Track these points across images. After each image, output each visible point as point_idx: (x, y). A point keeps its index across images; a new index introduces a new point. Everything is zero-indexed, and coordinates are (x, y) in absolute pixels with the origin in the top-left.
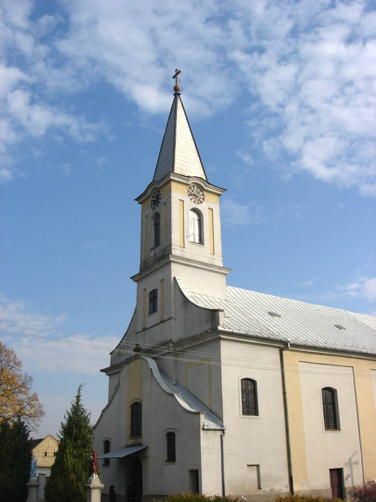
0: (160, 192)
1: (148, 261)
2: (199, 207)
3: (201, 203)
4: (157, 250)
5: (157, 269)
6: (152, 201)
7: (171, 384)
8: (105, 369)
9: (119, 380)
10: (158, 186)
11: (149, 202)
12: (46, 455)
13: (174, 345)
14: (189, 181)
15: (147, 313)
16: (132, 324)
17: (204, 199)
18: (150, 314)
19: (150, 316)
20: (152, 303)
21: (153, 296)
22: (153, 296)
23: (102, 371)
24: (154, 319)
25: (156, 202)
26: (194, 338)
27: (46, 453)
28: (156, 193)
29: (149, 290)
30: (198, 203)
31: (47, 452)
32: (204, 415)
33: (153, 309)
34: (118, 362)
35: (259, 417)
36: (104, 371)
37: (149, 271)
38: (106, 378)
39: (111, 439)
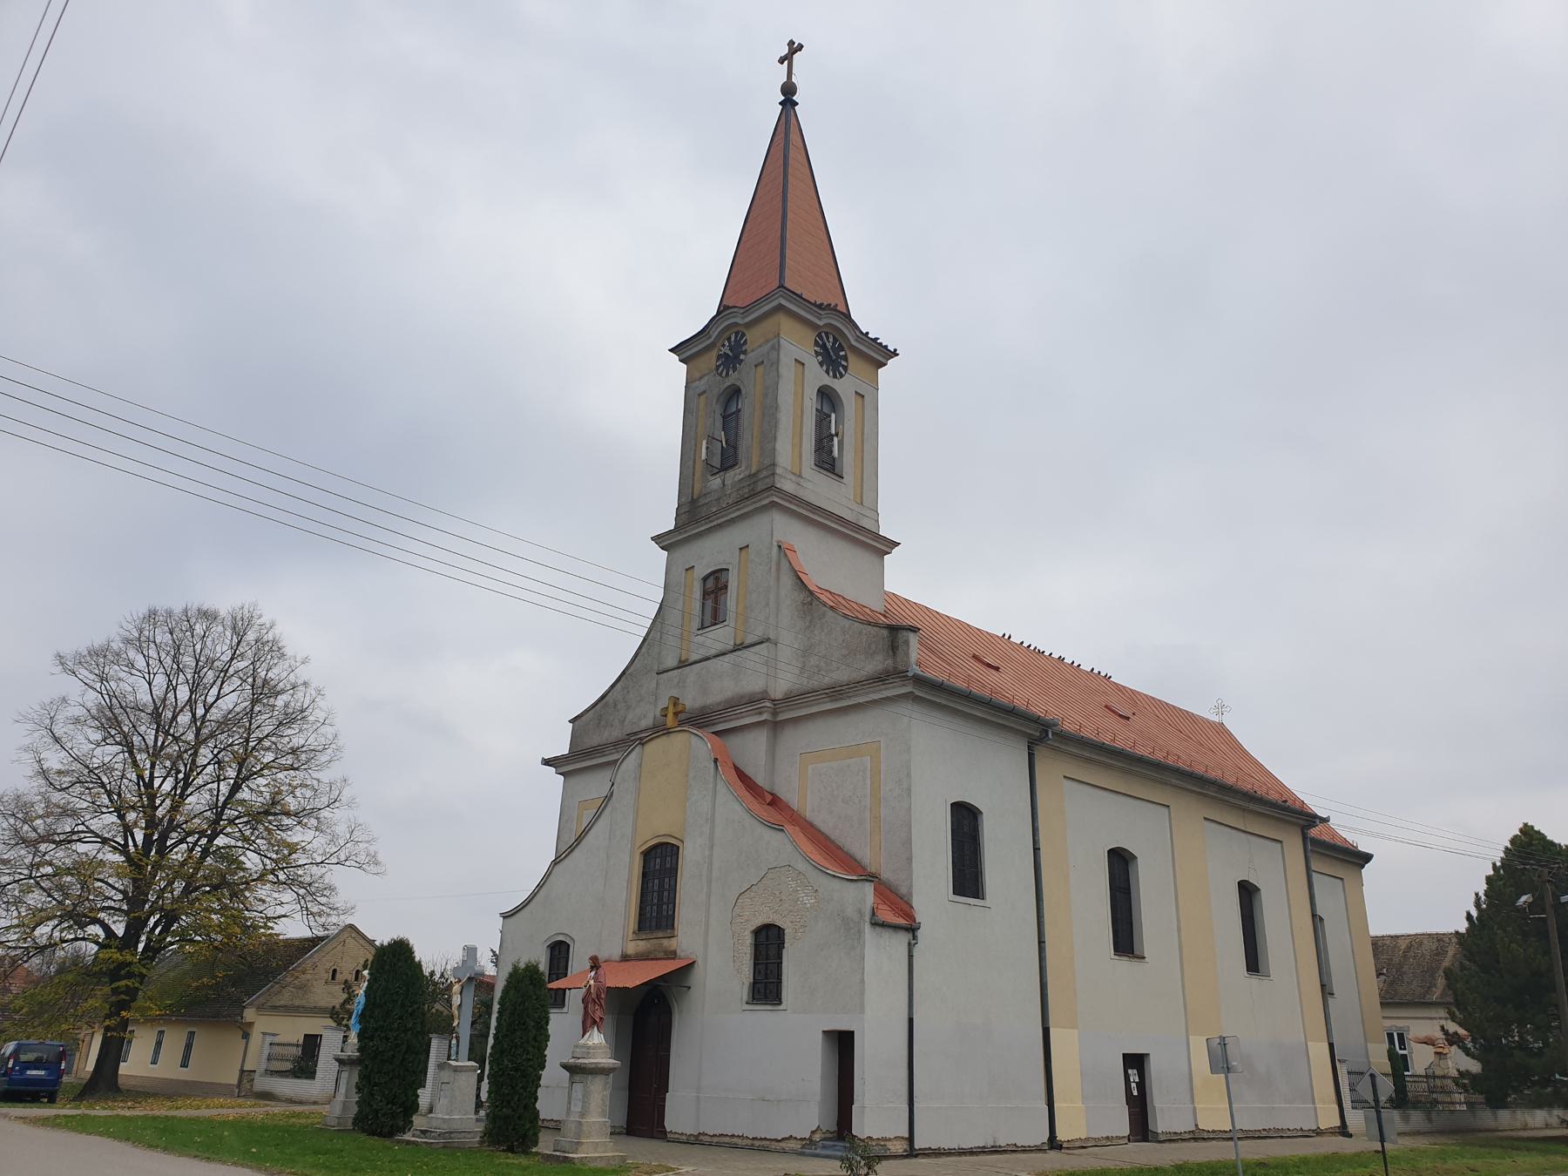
0: (743, 335)
1: (702, 502)
2: (837, 385)
3: (842, 376)
4: (733, 476)
5: (733, 521)
6: (719, 357)
7: (762, 801)
8: (556, 758)
9: (613, 785)
10: (741, 322)
11: (711, 360)
12: (333, 978)
13: (775, 705)
14: (820, 319)
15: (696, 623)
16: (643, 650)
17: (847, 367)
18: (703, 628)
19: (701, 632)
20: (709, 603)
21: (715, 586)
22: (715, 586)
23: (547, 762)
24: (720, 637)
25: (731, 360)
26: (835, 691)
27: (335, 971)
28: (733, 339)
29: (702, 570)
30: (835, 376)
31: (338, 969)
32: (872, 884)
33: (713, 616)
34: (595, 740)
35: (988, 902)
36: (551, 763)
37: (707, 523)
38: (554, 781)
39: (575, 938)
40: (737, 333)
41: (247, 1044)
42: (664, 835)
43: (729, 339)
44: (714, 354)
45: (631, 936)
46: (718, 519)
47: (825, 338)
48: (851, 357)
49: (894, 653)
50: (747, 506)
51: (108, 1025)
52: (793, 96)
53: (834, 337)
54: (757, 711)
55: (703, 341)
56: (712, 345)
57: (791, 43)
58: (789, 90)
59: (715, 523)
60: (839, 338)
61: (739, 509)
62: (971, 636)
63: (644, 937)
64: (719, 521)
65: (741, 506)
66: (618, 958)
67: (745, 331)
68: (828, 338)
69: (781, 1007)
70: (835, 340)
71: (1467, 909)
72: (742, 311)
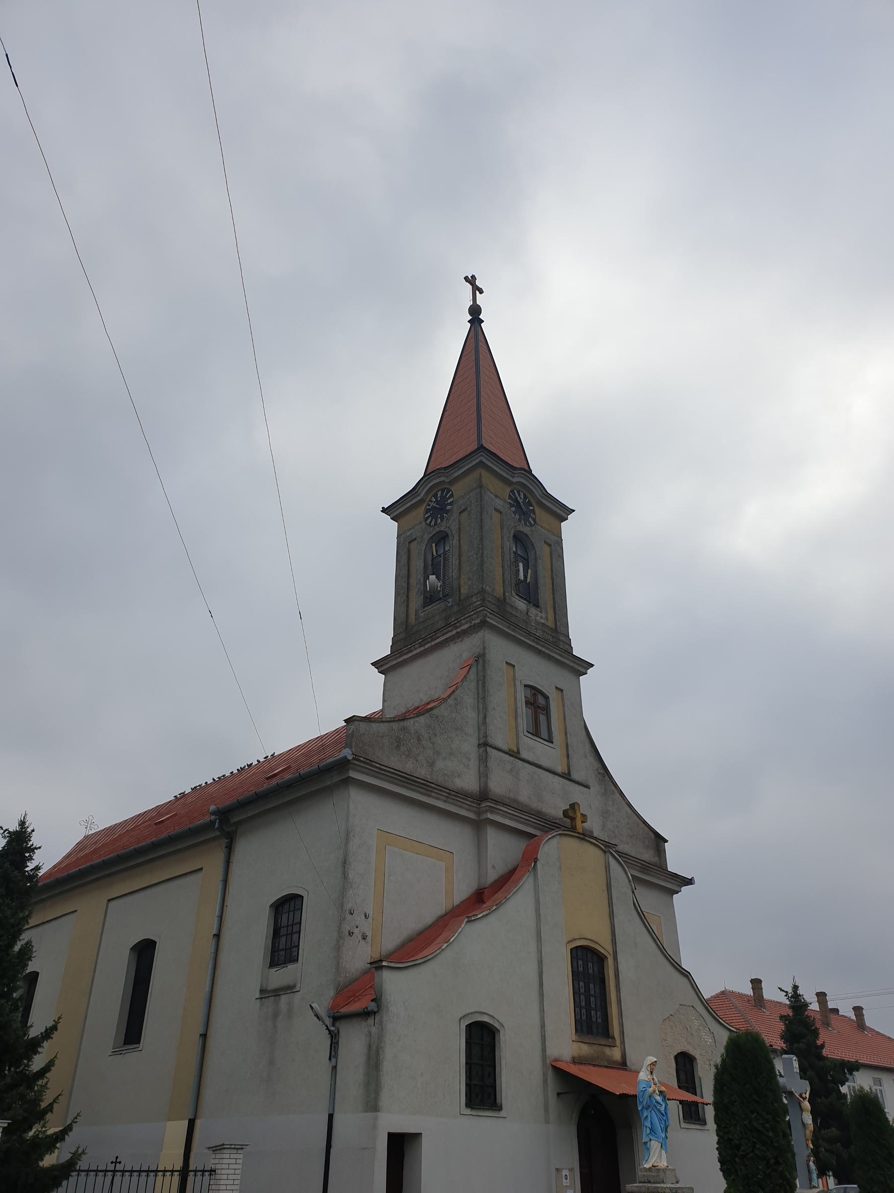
6: (427, 511)
25: (439, 510)
40: (443, 491)
41: (544, 1050)
43: (435, 496)
44: (422, 510)
46: (543, 646)
47: (517, 495)
48: (538, 510)
52: (480, 315)
53: (524, 495)
55: (509, 474)
56: (422, 501)
57: (466, 279)
58: (475, 311)
59: (540, 648)
60: (528, 495)
61: (561, 656)
62: (316, 744)
63: (588, 1041)
64: (543, 649)
65: (566, 656)
67: (450, 487)
68: (519, 495)
70: (525, 497)
71: (122, 1161)
72: (541, 493)
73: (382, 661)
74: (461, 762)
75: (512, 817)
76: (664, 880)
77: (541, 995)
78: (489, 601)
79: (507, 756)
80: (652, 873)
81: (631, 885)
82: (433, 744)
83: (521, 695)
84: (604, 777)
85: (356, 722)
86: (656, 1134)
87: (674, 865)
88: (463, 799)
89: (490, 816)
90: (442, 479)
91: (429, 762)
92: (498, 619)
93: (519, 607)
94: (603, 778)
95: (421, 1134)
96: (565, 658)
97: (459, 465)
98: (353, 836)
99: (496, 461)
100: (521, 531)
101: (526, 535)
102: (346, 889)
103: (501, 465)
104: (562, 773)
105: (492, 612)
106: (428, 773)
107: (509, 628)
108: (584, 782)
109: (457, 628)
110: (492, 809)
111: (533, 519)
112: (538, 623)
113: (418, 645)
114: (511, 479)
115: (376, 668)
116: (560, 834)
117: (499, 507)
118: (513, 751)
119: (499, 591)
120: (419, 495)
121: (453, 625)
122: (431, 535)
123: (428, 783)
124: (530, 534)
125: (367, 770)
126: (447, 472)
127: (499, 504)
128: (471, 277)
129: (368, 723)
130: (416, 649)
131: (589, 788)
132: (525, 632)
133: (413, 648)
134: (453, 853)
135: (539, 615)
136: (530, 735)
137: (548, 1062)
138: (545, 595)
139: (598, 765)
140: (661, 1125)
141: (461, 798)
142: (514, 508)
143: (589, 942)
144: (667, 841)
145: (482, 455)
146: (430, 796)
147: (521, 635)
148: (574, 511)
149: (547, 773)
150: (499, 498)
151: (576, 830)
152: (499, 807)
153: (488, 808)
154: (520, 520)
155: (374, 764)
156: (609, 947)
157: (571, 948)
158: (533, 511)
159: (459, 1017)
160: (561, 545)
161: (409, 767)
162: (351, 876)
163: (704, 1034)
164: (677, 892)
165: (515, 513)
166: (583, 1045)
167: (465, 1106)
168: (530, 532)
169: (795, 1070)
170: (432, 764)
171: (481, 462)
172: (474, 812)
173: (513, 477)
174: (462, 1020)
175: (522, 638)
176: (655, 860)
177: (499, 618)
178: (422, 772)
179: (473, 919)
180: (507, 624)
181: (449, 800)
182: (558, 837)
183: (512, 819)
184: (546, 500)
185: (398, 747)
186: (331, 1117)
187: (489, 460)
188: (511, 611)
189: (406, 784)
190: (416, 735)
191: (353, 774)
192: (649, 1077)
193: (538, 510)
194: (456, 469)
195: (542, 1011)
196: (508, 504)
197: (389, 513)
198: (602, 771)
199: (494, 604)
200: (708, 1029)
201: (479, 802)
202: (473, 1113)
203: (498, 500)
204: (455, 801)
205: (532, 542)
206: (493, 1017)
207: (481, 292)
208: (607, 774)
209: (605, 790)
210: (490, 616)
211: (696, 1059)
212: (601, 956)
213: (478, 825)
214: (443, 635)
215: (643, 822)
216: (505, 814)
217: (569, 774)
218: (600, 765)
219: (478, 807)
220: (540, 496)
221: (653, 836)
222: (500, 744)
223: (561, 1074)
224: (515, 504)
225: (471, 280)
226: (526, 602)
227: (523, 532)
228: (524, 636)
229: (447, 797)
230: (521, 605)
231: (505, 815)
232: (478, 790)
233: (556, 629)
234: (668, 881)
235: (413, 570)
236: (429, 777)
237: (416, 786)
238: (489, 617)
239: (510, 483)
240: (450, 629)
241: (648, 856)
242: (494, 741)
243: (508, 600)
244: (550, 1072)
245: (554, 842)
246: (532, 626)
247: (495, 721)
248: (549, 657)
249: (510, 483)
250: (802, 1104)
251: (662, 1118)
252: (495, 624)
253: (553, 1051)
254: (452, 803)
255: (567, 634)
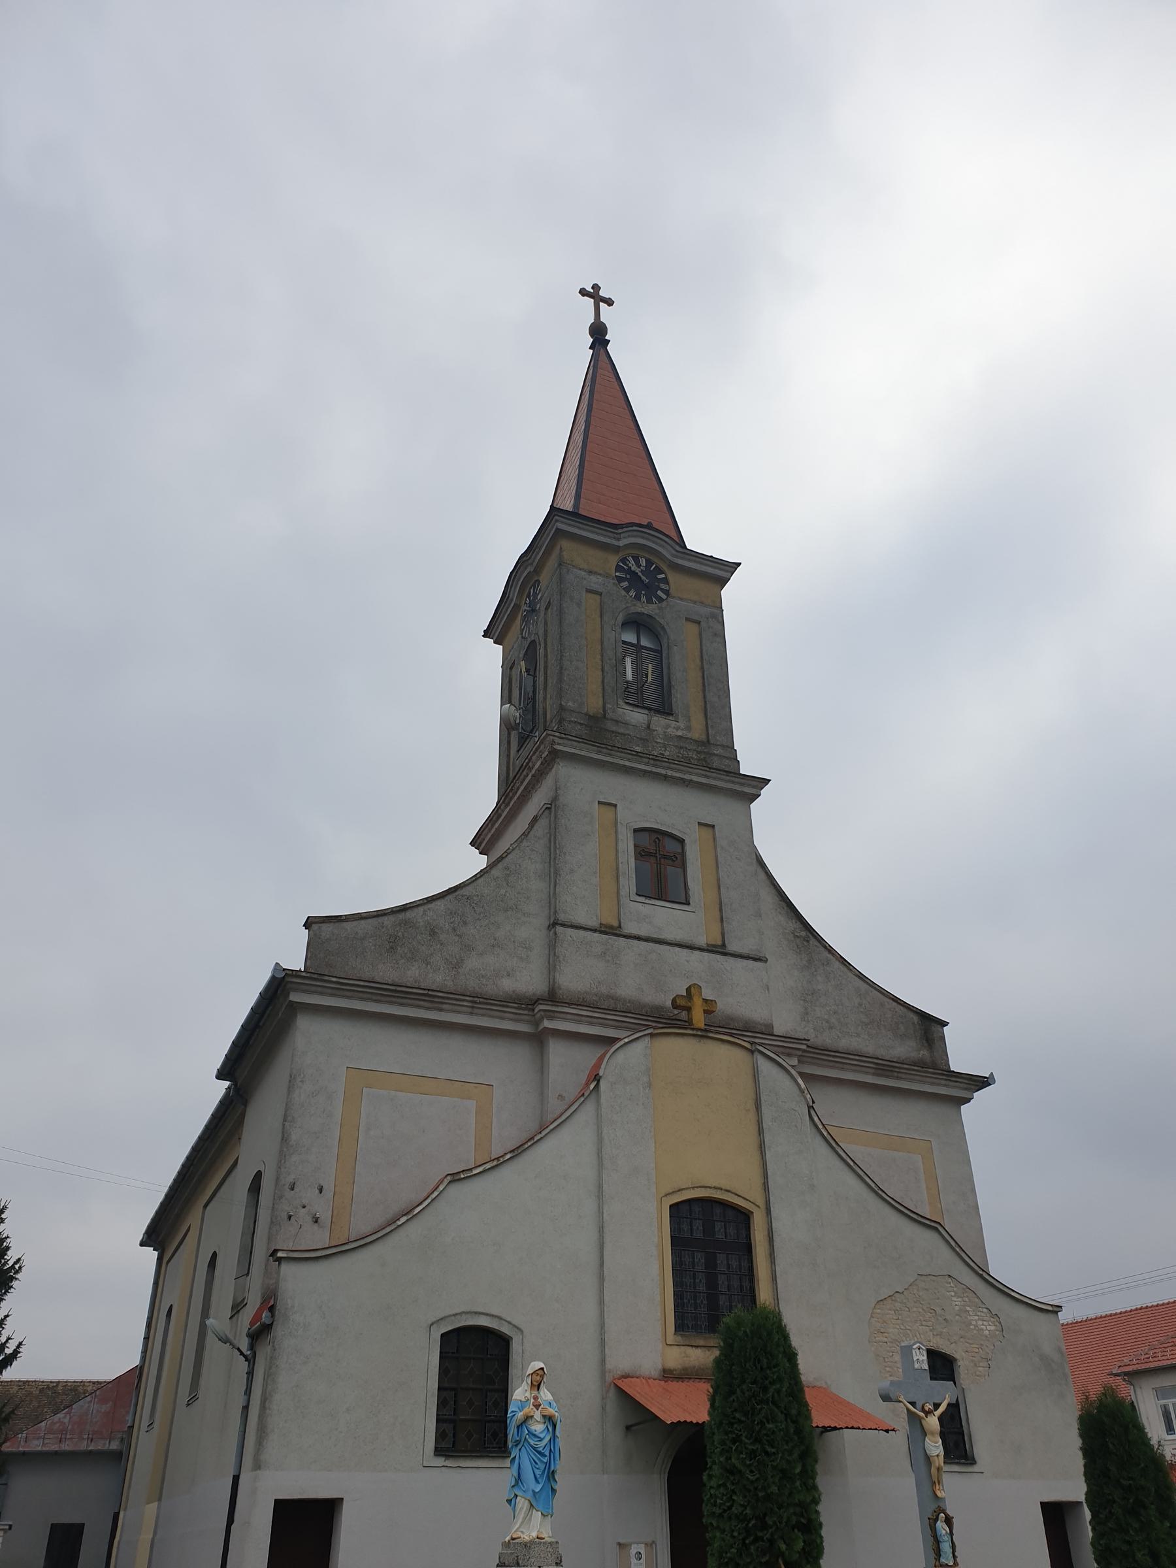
42: (715, 1188)
45: (671, 1338)
46: (668, 768)
48: (673, 577)
49: (929, 1045)
50: (719, 779)
51: (778, 1508)
54: (788, 1051)
55: (609, 537)
58: (599, 333)
61: (708, 777)
63: (702, 1343)
64: (669, 773)
65: (714, 775)
66: (655, 1374)
69: (976, 1468)
72: (674, 552)
73: (479, 838)
74: (603, 955)
75: (591, 1021)
76: (932, 1084)
77: (601, 1279)
78: (570, 722)
79: (597, 935)
80: (903, 1076)
81: (805, 1098)
82: (460, 936)
83: (627, 845)
84: (808, 941)
85: (313, 925)
86: (523, 1485)
87: (960, 1060)
88: (503, 1006)
89: (547, 1024)
90: (528, 570)
91: (451, 963)
92: (576, 744)
93: (633, 721)
94: (805, 943)
95: (343, 1499)
96: (714, 778)
97: (538, 544)
98: (302, 1081)
99: (582, 523)
100: (639, 613)
101: (650, 616)
102: (285, 1156)
103: (591, 526)
104: (708, 945)
105: (563, 736)
106: (447, 978)
107: (599, 752)
108: (753, 954)
109: (530, 769)
110: (552, 1014)
111: (664, 591)
112: (667, 737)
113: (504, 805)
114: (616, 543)
115: (476, 848)
116: (651, 1035)
117: (595, 587)
118: (612, 927)
119: (594, 704)
120: (512, 600)
121: (526, 766)
122: (525, 651)
123: (430, 993)
124: (656, 614)
125: (319, 989)
126: (530, 558)
127: (595, 582)
128: (593, 288)
129: (337, 924)
130: (503, 811)
131: (766, 961)
132: (630, 754)
133: (500, 811)
134: (492, 1085)
135: (673, 726)
136: (642, 899)
137: (609, 1378)
138: (686, 693)
139: (793, 925)
140: (536, 1470)
141: (496, 1005)
142: (627, 583)
143: (714, 1191)
144: (945, 1024)
145: (557, 521)
146: (441, 1010)
147: (623, 758)
148: (739, 564)
149: (677, 949)
150: (596, 573)
151: (692, 1024)
152: (560, 1009)
153: (542, 1013)
154: (638, 597)
155: (327, 978)
156: (757, 1196)
157: (672, 1203)
158: (665, 581)
159: (430, 1323)
160: (720, 619)
161: (412, 974)
162: (294, 1137)
163: (976, 1318)
164: (968, 1100)
165: (627, 590)
166: (690, 1351)
167: (432, 1454)
168: (657, 611)
169: (917, 1366)
170: (456, 965)
171: (558, 530)
172: (529, 1022)
173: (619, 540)
174: (435, 1325)
175: (627, 763)
176: (924, 1053)
177: (579, 742)
178: (438, 978)
179: (462, 1176)
180: (595, 748)
181: (476, 1011)
182: (647, 1039)
183: (592, 1024)
184: (685, 559)
185: (392, 950)
186: (236, 1480)
187: (570, 525)
188: (614, 729)
189: (394, 999)
190: (428, 928)
191: (295, 997)
192: (528, 1394)
193: (673, 577)
194: (537, 550)
195: (601, 1302)
196: (613, 579)
197: (491, 636)
198: (803, 934)
199: (581, 724)
200: (985, 1310)
201: (530, 1007)
202: (449, 1463)
203: (593, 578)
204: (488, 1012)
205: (661, 624)
206: (500, 1318)
207: (610, 302)
208: (813, 935)
209: (809, 961)
210: (561, 741)
211: (956, 1360)
212: (740, 1209)
213: (539, 1039)
214: (522, 783)
215: (893, 999)
216: (576, 1017)
217: (724, 945)
218: (798, 925)
219: (531, 1013)
220: (673, 556)
221: (915, 1018)
222: (581, 918)
223: (625, 1398)
224: (628, 576)
225: (594, 294)
226: (646, 712)
227: (644, 613)
228: (629, 760)
229: (473, 1007)
230: (637, 717)
231: (578, 1019)
232: (547, 989)
233: (708, 741)
234: (938, 1085)
235: (701, 717)
236: (450, 983)
237: (410, 998)
238: (559, 744)
239: (616, 549)
240: (525, 773)
241: (905, 1049)
242: (572, 917)
243: (610, 714)
244: (612, 1393)
245: (639, 1048)
246: (657, 743)
247: (575, 888)
248: (684, 782)
249: (616, 549)
250: (923, 1422)
251: (539, 1459)
252: (573, 751)
253: (619, 1362)
254: (483, 1015)
255: (730, 745)
